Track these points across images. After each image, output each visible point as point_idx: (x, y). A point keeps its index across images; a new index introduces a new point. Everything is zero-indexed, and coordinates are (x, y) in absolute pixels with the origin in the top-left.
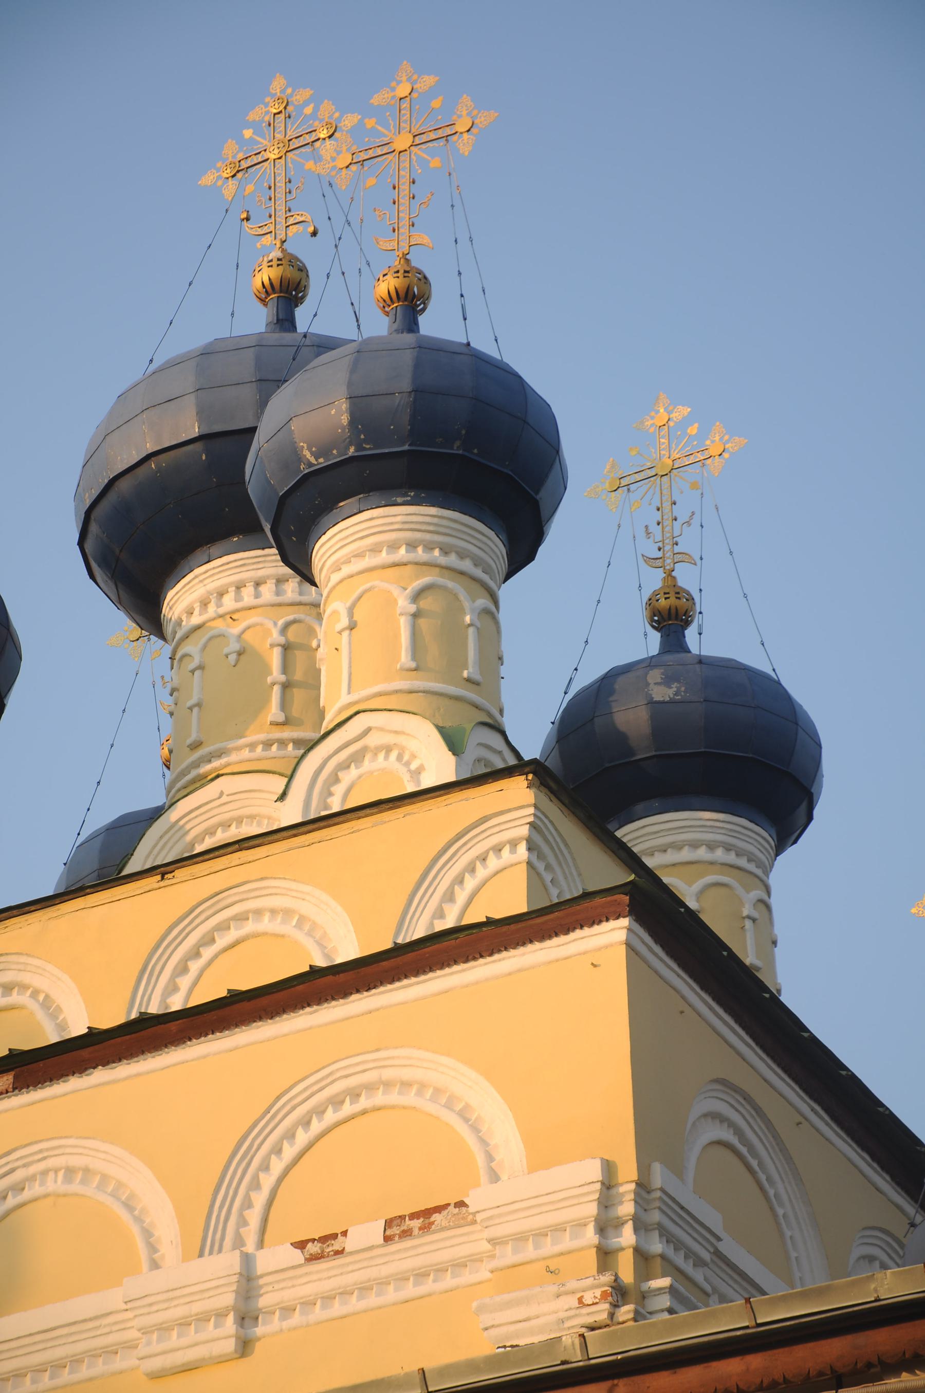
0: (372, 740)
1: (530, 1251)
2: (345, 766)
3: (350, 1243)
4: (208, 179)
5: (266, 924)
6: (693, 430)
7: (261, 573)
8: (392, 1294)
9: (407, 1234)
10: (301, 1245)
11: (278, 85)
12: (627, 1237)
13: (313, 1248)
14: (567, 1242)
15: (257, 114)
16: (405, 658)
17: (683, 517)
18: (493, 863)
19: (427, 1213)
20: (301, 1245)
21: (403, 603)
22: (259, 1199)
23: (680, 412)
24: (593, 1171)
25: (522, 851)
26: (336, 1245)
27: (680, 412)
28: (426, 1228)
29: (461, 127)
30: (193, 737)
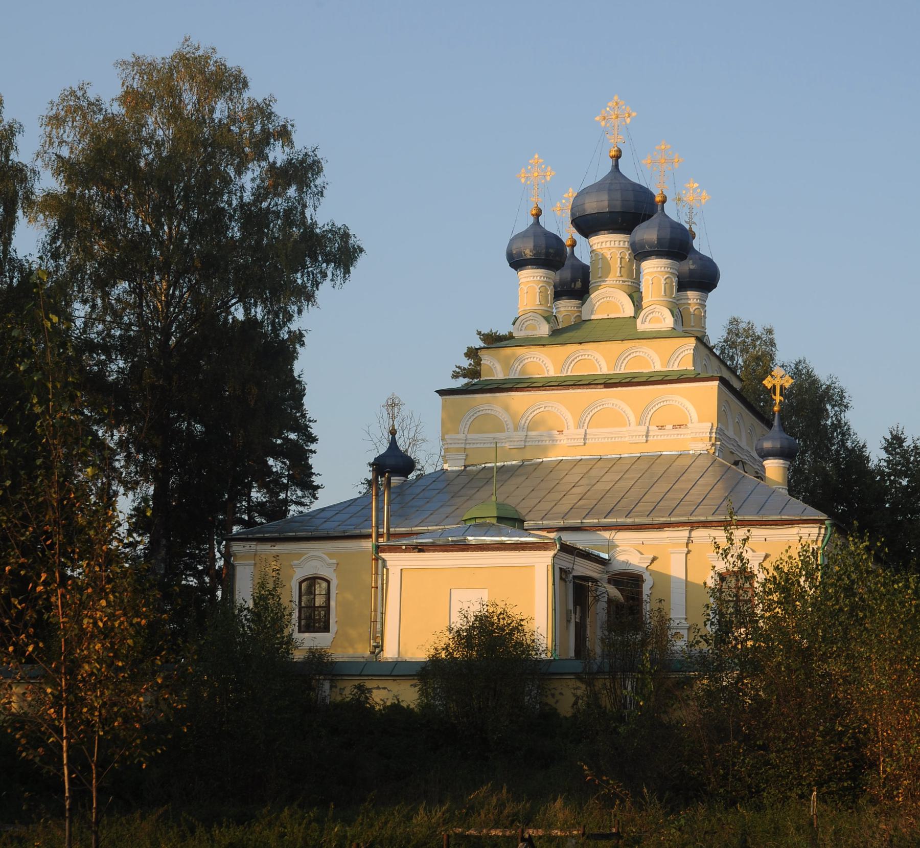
0: (655, 310)
1: (698, 435)
2: (650, 314)
3: (666, 428)
4: (597, 118)
5: (641, 354)
6: (699, 191)
7: (616, 239)
8: (672, 437)
9: (676, 428)
10: (658, 426)
11: (616, 98)
12: (714, 435)
13: (660, 428)
14: (704, 435)
15: (610, 104)
16: (663, 293)
17: (695, 213)
18: (686, 352)
19: (680, 425)
20: (658, 426)
21: (663, 281)
22: (649, 416)
23: (696, 185)
24: (710, 425)
25: (692, 351)
26: (664, 428)
27: (696, 185)
28: (680, 428)
29: (676, 160)
30: (599, 276)
